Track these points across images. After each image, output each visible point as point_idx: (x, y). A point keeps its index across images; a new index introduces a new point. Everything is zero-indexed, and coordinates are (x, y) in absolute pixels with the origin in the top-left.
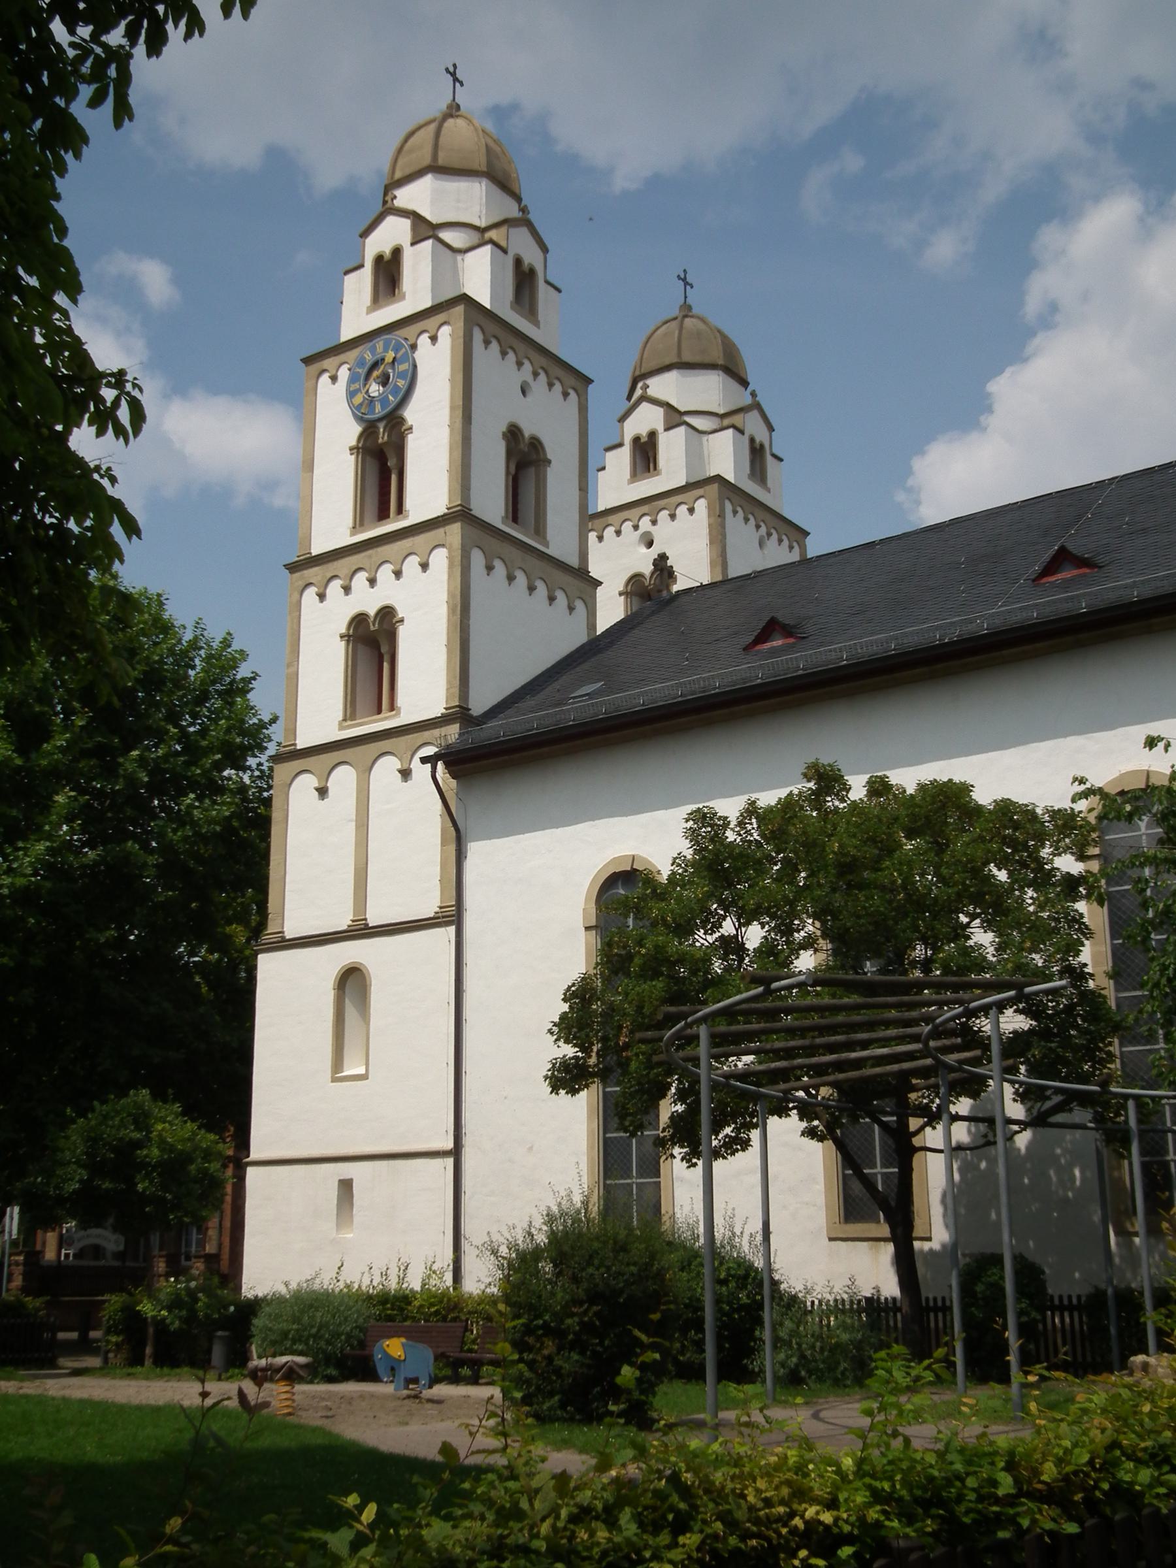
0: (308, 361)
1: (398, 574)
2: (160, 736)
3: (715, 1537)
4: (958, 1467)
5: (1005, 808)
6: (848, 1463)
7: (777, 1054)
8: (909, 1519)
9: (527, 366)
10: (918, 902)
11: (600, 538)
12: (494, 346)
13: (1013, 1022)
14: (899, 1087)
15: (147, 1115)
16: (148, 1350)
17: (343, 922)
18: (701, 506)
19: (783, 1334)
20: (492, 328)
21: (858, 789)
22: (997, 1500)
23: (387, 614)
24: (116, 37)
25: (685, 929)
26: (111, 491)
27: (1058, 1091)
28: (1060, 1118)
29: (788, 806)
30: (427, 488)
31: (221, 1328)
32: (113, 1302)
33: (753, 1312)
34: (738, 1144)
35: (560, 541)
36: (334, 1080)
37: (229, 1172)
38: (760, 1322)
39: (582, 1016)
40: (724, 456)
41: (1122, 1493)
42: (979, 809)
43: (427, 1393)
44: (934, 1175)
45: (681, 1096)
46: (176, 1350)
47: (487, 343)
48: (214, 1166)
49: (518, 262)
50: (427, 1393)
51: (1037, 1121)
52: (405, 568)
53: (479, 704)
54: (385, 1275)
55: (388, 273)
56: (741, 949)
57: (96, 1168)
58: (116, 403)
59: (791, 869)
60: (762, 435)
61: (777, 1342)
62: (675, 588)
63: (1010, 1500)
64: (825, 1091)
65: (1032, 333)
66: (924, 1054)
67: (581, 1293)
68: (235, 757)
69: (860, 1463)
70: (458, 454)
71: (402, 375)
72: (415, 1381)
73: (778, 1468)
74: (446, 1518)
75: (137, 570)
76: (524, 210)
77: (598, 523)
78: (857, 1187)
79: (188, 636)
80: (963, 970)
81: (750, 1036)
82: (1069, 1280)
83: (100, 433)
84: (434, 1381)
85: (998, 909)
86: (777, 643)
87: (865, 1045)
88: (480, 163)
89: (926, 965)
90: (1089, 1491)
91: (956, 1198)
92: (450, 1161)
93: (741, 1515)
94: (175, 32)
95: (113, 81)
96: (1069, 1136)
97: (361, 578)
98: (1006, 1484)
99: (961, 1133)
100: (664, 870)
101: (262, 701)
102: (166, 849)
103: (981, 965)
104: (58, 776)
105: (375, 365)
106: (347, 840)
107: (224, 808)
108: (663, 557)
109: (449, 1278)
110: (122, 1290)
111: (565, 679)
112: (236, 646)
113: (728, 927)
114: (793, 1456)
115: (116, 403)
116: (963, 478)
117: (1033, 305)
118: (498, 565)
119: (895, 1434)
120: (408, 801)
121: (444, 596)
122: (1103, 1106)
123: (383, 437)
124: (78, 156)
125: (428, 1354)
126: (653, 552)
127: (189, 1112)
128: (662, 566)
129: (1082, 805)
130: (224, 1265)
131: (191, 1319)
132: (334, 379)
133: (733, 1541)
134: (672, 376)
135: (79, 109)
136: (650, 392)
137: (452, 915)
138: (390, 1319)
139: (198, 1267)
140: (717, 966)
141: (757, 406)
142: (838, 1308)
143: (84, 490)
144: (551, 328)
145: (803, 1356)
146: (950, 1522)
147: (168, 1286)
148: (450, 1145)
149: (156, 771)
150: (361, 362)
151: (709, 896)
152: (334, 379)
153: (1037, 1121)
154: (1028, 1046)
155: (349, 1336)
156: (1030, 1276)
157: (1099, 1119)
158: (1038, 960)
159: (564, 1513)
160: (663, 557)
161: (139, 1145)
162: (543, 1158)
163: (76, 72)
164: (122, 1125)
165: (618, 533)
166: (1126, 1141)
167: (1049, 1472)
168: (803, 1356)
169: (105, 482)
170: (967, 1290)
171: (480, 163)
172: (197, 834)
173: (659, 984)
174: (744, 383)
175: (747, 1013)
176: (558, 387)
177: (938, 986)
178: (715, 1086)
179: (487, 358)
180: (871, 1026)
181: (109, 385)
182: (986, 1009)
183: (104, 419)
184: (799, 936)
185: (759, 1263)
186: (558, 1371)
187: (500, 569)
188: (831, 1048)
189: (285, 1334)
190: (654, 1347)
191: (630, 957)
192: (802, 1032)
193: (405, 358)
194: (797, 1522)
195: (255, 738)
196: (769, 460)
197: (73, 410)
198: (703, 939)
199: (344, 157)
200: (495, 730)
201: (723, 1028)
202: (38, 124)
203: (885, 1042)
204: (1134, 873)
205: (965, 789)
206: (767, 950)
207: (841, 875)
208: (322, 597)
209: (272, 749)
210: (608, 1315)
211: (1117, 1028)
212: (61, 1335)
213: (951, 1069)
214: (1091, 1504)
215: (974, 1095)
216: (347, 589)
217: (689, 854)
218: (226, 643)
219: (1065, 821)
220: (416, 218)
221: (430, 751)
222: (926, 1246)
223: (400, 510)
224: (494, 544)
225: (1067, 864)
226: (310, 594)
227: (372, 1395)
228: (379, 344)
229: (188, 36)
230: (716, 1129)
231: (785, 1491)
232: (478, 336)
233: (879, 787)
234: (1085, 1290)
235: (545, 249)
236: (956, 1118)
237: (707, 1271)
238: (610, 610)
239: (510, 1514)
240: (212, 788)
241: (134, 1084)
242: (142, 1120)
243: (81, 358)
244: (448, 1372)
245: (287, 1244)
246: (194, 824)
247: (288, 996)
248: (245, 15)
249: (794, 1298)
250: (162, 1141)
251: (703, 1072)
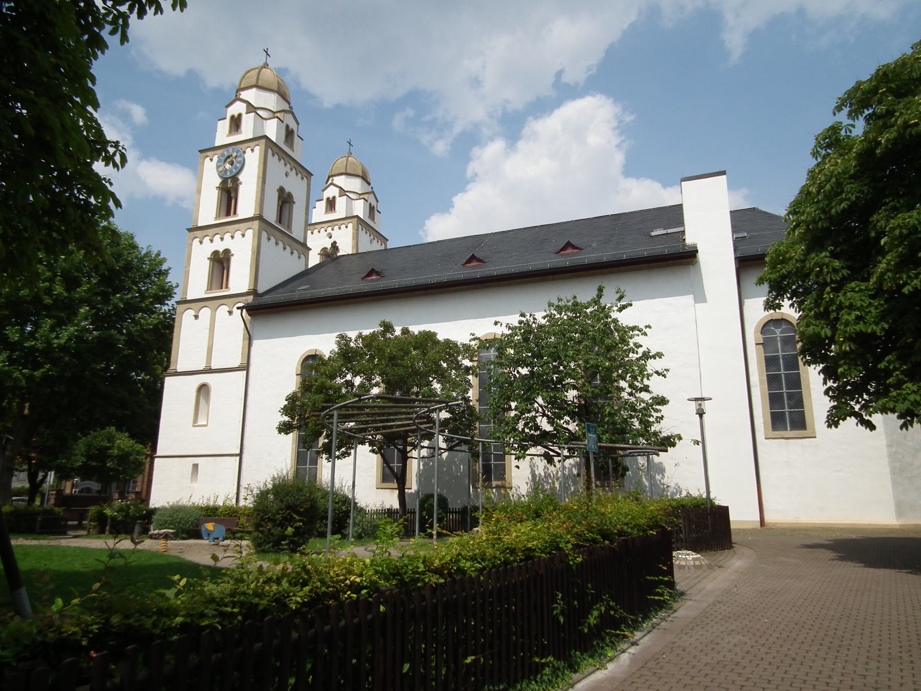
0: (201, 151)
1: (232, 237)
2: (130, 290)
3: (317, 587)
4: (406, 562)
5: (448, 342)
6: (368, 561)
7: (362, 422)
8: (387, 580)
10: (416, 373)
12: (276, 156)
13: (444, 415)
14: (404, 436)
15: (113, 437)
16: (107, 528)
17: (202, 367)
18: (350, 225)
19: (357, 521)
20: (275, 149)
21: (398, 332)
22: (419, 573)
23: (227, 251)
24: (124, 8)
25: (333, 377)
26: (110, 188)
27: (458, 439)
28: (457, 448)
29: (373, 335)
30: (246, 206)
31: (140, 519)
32: (93, 509)
33: (347, 514)
34: (346, 454)
35: (297, 231)
37: (148, 460)
38: (349, 517)
39: (292, 406)
40: (359, 208)
41: (461, 571)
42: (439, 341)
43: (222, 543)
44: (414, 467)
45: (327, 437)
46: (120, 528)
47: (273, 155)
48: (140, 458)
49: (287, 126)
50: (222, 543)
51: (450, 449)
52: (235, 235)
53: (261, 289)
54: (208, 499)
55: (236, 123)
56: (352, 385)
57: (90, 457)
58: (114, 154)
59: (372, 357)
60: (374, 203)
61: (355, 524)
62: (339, 254)
63: (423, 573)
64: (379, 437)
65: (468, 182)
66: (414, 424)
67: (283, 506)
68: (161, 300)
69: (372, 561)
70: (259, 195)
71: (239, 162)
72: (217, 539)
73: (343, 563)
74: (214, 583)
75: (120, 221)
76: (291, 108)
77: (312, 227)
78: (387, 471)
79: (144, 252)
80: (429, 396)
81: (353, 416)
82: (455, 503)
83: (107, 165)
84: (225, 539)
85: (442, 376)
86: (374, 277)
87: (394, 420)
88: (275, 87)
89: (417, 394)
90: (449, 570)
91: (420, 475)
92: (238, 458)
93: (327, 580)
94: (150, 11)
95: (121, 26)
96: (460, 454)
97: (217, 237)
98: (422, 568)
99: (424, 452)
100: (327, 355)
101: (172, 279)
102: (129, 334)
103: (435, 395)
104: (82, 301)
105: (229, 157)
106: (204, 336)
107: (153, 320)
108: (335, 242)
109: (234, 501)
110: (98, 504)
111: (295, 283)
112: (162, 256)
113: (349, 377)
114: (348, 559)
115: (114, 154)
116: (442, 228)
117: (469, 173)
119: (386, 551)
120: (231, 324)
121: (251, 248)
122: (471, 444)
123: (230, 185)
124: (103, 53)
125: (224, 529)
126: (332, 241)
127: (132, 436)
128: (334, 245)
129: (473, 343)
130: (143, 496)
131: (127, 515)
132: (211, 160)
133: (323, 589)
135: (105, 33)
137: (245, 367)
138: (210, 516)
139: (132, 496)
140: (344, 391)
141: (373, 193)
142: (377, 512)
143: (98, 187)
144: (297, 154)
145: (363, 529)
146: (402, 581)
147: (118, 503)
149: (127, 303)
150: (223, 155)
151: (343, 365)
152: (211, 160)
153: (450, 449)
154: (449, 423)
155: (192, 522)
156: (443, 501)
157: (470, 449)
158: (454, 394)
159: (261, 580)
160: (335, 242)
161: (109, 448)
162: (273, 457)
163: (104, 19)
164: (102, 440)
166: (478, 457)
167: (437, 563)
168: (363, 529)
169: (108, 185)
170: (422, 507)
171: (275, 87)
172: (142, 329)
173: (322, 396)
174: (369, 184)
175: (351, 407)
176: (300, 175)
177: (419, 401)
178: (339, 434)
179: (273, 161)
180: (396, 414)
181: (111, 146)
182: (435, 410)
183: (109, 160)
184: (374, 382)
185: (350, 497)
186: (272, 534)
187: (273, 240)
188: (382, 421)
189: (166, 522)
190: (300, 521)
191: (312, 386)
192: (373, 415)
193: (241, 156)
194: (348, 582)
195: (165, 293)
197: (95, 154)
198: (339, 381)
199: (221, 74)
200: (268, 299)
201: (344, 412)
202: (86, 37)
203: (400, 420)
204: (488, 367)
205: (435, 334)
206: (362, 386)
207: (390, 361)
208: (201, 242)
209: (177, 298)
210: (294, 514)
211: (478, 419)
212: (70, 523)
213: (423, 430)
214: (450, 574)
215: (430, 440)
216: (212, 241)
217: (336, 350)
218: (158, 255)
219: (467, 348)
221: (241, 305)
222: (410, 491)
223: (235, 213)
224: (272, 231)
225: (467, 363)
226: (196, 241)
227: (199, 544)
228: (230, 149)
229: (156, 13)
230: (339, 448)
231: (344, 571)
232: (270, 152)
233: (405, 331)
234: (461, 507)
235: (298, 124)
236: (423, 447)
237: (330, 499)
238: (314, 259)
239: (240, 581)
240: (150, 311)
241: (109, 424)
242: (111, 439)
243: (100, 133)
244: (230, 535)
245: (169, 487)
246: (141, 324)
247: (176, 394)
248: (182, 10)
249: (362, 509)
250: (119, 447)
251: (334, 428)
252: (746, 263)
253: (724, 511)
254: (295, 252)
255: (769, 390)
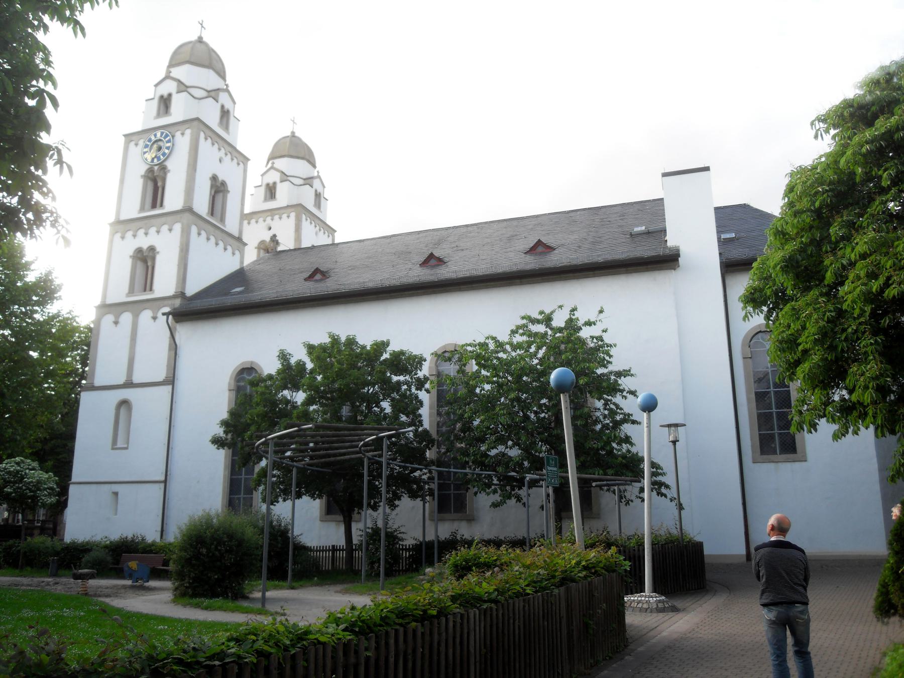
9: (223, 150)
11: (249, 223)
12: (209, 140)
17: (121, 380)
23: (152, 249)
30: (173, 199)
36: (113, 449)
47: (206, 139)
53: (190, 291)
60: (320, 190)
71: (168, 148)
87: (337, 448)
92: (162, 485)
97: (141, 232)
108: (275, 236)
118: (203, 233)
126: (271, 233)
128: (274, 239)
132: (136, 145)
134: (285, 160)
136: (275, 166)
141: (319, 177)
148: (163, 478)
160: (275, 236)
162: (202, 487)
165: (257, 222)
176: (235, 160)
179: (205, 146)
196: (322, 199)
220: (179, 82)
223: (161, 205)
238: (251, 256)
252: (731, 266)
253: (699, 546)
254: (229, 248)
255: (758, 408)
